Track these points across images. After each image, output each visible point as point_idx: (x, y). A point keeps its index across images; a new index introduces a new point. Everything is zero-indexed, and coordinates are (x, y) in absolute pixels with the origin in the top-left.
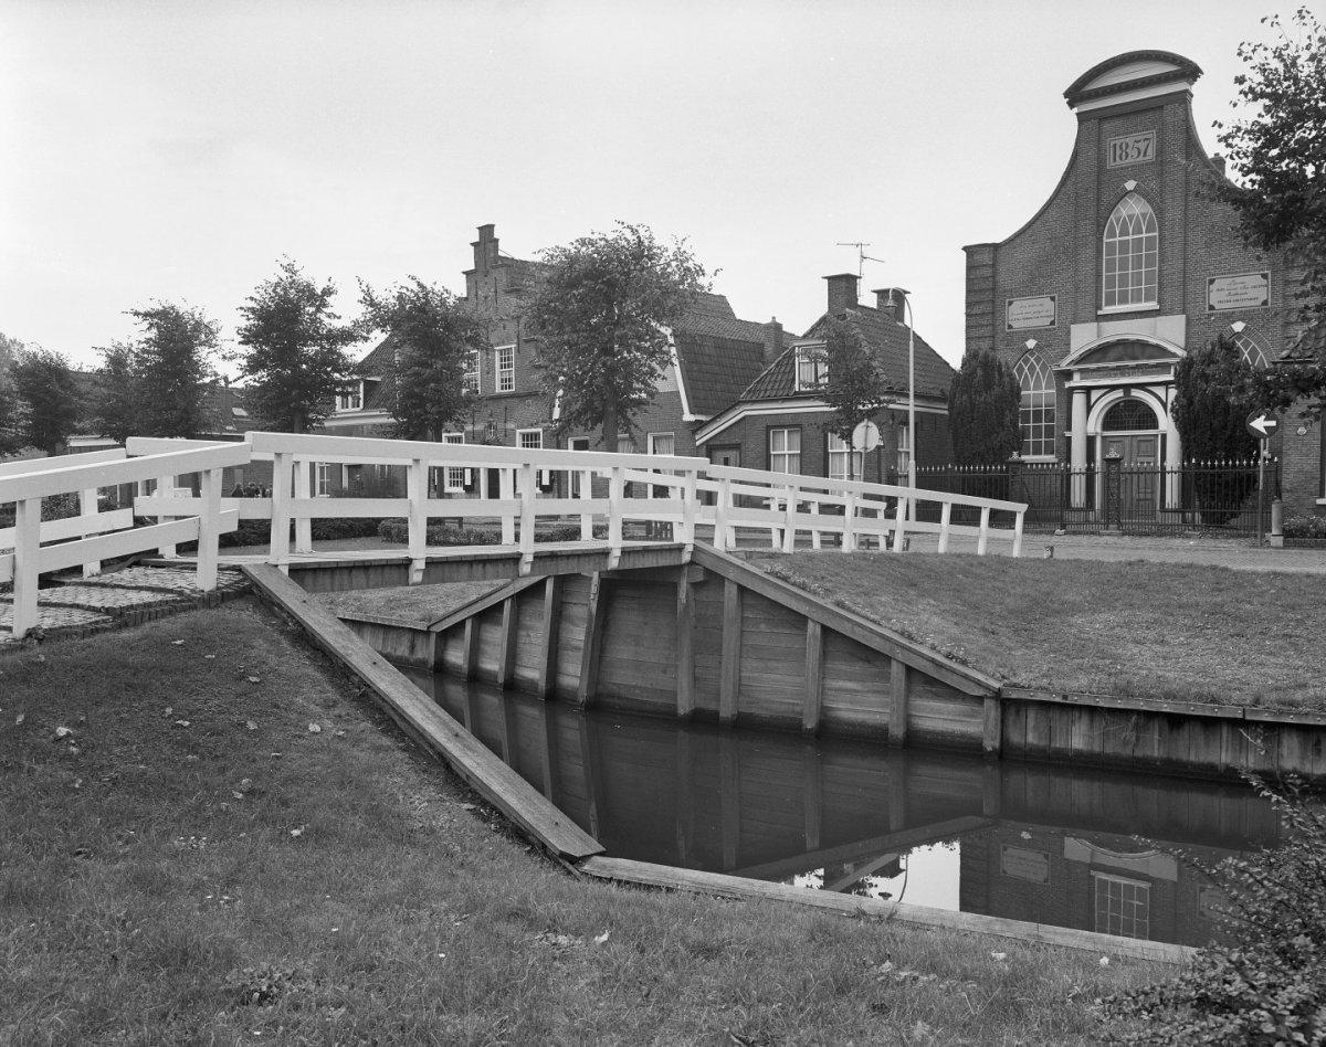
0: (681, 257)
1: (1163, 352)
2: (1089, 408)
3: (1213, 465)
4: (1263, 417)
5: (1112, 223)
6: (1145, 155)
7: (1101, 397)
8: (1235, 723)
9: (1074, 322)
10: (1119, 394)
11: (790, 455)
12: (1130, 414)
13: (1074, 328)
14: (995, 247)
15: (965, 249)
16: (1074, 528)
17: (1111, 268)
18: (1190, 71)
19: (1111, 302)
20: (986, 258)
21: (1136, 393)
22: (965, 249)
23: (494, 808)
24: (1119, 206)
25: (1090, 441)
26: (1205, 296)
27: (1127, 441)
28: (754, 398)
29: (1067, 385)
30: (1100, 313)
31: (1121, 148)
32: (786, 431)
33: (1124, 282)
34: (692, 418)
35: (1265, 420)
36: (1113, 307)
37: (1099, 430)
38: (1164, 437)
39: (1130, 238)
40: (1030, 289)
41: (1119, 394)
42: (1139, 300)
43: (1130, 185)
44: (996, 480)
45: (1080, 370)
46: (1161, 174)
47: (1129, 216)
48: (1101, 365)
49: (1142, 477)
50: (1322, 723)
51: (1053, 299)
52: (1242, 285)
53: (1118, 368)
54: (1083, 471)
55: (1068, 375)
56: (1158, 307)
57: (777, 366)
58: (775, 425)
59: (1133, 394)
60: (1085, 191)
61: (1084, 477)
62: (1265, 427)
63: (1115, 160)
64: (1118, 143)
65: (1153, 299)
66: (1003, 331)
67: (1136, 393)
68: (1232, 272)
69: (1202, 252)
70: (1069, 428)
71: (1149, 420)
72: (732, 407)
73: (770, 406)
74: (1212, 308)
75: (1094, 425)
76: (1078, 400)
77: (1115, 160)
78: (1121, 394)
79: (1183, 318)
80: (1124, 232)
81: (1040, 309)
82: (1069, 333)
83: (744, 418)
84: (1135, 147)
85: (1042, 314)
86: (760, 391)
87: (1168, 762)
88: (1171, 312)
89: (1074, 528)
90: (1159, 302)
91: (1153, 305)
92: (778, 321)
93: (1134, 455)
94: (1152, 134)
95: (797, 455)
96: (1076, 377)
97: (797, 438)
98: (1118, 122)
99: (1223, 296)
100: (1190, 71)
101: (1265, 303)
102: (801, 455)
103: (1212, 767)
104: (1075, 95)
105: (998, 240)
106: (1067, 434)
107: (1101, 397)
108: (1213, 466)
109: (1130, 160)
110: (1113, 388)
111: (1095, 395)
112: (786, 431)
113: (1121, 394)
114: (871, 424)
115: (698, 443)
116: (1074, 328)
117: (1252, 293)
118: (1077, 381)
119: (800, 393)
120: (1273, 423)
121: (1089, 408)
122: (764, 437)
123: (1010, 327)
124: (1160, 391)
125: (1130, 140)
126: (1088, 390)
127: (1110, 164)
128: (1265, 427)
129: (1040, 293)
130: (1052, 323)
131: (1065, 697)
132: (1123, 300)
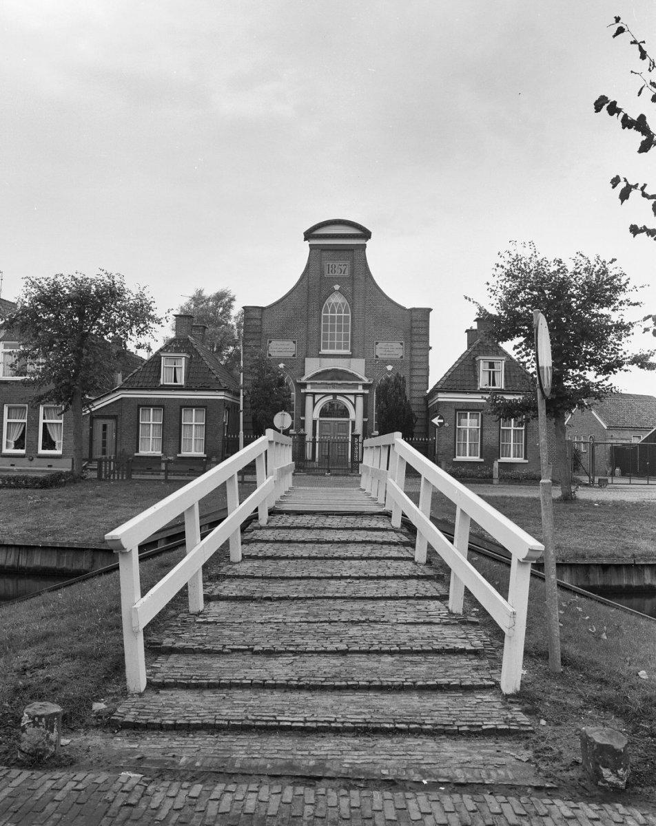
0: (141, 296)
2: (314, 405)
5: (326, 306)
7: (321, 398)
8: (628, 566)
9: (307, 357)
10: (330, 398)
11: (196, 425)
12: (334, 410)
13: (307, 360)
14: (263, 309)
16: (335, 472)
17: (326, 329)
18: (366, 235)
19: (325, 348)
20: (257, 314)
21: (339, 398)
23: (227, 653)
25: (314, 422)
27: (332, 424)
29: (303, 391)
30: (320, 353)
31: (332, 267)
32: (152, 409)
33: (332, 338)
37: (318, 417)
38: (354, 423)
39: (336, 315)
40: (282, 335)
41: (330, 398)
42: (334, 348)
45: (311, 383)
46: (353, 285)
48: (322, 381)
49: (340, 444)
50: (655, 563)
51: (294, 342)
53: (332, 384)
54: (311, 440)
55: (304, 385)
58: (147, 404)
60: (311, 288)
63: (329, 273)
64: (331, 264)
65: (348, 349)
69: (372, 327)
70: (303, 415)
71: (345, 413)
73: (129, 392)
74: (377, 357)
75: (316, 415)
76: (309, 400)
77: (329, 273)
78: (332, 398)
80: (333, 311)
81: (288, 347)
82: (304, 362)
83: (121, 398)
84: (340, 268)
87: (603, 586)
88: (358, 357)
89: (335, 472)
91: (347, 352)
94: (348, 263)
100: (366, 235)
101: (402, 357)
103: (620, 587)
104: (308, 235)
105: (264, 305)
107: (321, 398)
111: (317, 397)
112: (194, 410)
113: (332, 398)
114: (286, 413)
116: (307, 360)
118: (309, 389)
120: (442, 421)
121: (314, 405)
124: (352, 398)
125: (337, 264)
126: (314, 394)
127: (326, 275)
129: (287, 338)
130: (294, 356)
131: (563, 561)
132: (339, 348)
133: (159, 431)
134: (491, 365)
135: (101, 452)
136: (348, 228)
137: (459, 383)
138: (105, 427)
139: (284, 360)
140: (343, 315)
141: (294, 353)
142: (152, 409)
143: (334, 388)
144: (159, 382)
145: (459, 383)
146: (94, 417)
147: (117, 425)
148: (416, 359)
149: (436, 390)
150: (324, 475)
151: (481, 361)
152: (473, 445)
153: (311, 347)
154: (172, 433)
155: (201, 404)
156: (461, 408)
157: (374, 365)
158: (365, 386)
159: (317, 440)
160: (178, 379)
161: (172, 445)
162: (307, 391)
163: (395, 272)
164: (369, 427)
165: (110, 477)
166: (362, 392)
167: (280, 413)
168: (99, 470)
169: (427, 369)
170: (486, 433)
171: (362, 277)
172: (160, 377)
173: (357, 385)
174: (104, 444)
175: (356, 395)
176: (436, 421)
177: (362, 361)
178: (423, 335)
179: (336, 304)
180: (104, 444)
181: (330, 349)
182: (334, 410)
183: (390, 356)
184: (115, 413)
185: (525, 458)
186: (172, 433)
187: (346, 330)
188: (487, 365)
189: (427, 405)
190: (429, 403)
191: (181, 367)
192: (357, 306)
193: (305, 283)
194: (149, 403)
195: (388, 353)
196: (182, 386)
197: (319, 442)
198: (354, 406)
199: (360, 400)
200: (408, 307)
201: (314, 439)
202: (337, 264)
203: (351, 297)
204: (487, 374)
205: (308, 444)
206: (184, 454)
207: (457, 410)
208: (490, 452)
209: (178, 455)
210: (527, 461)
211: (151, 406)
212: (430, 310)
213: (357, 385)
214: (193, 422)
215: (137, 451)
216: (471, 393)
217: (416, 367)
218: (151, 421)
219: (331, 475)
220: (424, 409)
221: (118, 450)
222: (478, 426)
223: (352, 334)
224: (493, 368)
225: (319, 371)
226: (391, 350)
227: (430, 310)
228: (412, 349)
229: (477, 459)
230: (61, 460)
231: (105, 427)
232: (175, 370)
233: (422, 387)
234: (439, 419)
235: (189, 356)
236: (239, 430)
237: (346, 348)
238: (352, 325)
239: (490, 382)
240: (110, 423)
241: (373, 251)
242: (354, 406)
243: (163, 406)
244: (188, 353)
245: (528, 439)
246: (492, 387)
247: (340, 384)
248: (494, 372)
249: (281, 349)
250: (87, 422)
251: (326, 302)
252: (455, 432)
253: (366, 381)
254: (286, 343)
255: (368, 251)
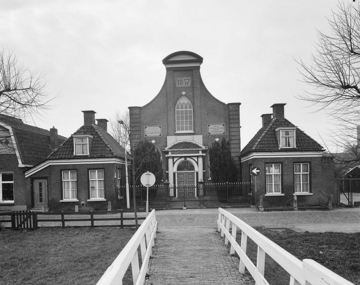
1: (196, 146)
2: (174, 164)
3: (235, 184)
4: (256, 169)
6: (188, 84)
9: (168, 135)
10: (183, 159)
11: (99, 180)
12: (185, 166)
13: (168, 137)
15: (129, 108)
19: (179, 130)
20: (137, 111)
21: (188, 159)
22: (129, 108)
24: (180, 99)
25: (174, 174)
26: (207, 130)
27: (185, 174)
28: (54, 158)
29: (166, 156)
30: (176, 133)
32: (69, 172)
34: (23, 166)
35: (257, 170)
36: (188, 131)
37: (176, 171)
38: (197, 173)
40: (152, 123)
41: (183, 159)
43: (184, 93)
44: (153, 190)
45: (171, 151)
46: (193, 91)
47: (183, 103)
51: (160, 127)
52: (218, 127)
54: (173, 187)
55: (167, 153)
56: (194, 132)
57: (64, 144)
58: (66, 168)
59: (187, 159)
60: (169, 93)
61: (173, 189)
62: (257, 172)
63: (178, 85)
66: (144, 137)
67: (188, 159)
68: (214, 123)
70: (168, 170)
72: (44, 161)
74: (209, 133)
75: (175, 169)
76: (170, 161)
78: (184, 159)
79: (202, 136)
80: (182, 108)
82: (166, 138)
84: (185, 81)
85: (157, 132)
86: (57, 155)
90: (194, 131)
91: (192, 131)
92: (56, 128)
93: (187, 179)
94: (190, 78)
95: (103, 180)
96: (170, 153)
97: (75, 175)
98: (179, 73)
99: (212, 130)
100: (199, 60)
101: (224, 133)
102: (77, 181)
104: (166, 61)
105: (141, 106)
106: (167, 172)
108: (222, 185)
109: (183, 85)
110: (181, 157)
112: (97, 171)
114: (150, 173)
115: (26, 177)
116: (168, 137)
117: (221, 130)
118: (170, 155)
119: (76, 156)
120: (259, 171)
121: (174, 164)
122: (59, 174)
123: (146, 136)
124: (196, 159)
125: (183, 79)
126: (173, 158)
127: (177, 86)
128: (257, 172)
129: (155, 125)
130: (160, 135)
132: (183, 130)
133: (75, 184)
134: (287, 133)
135: (39, 200)
136: (189, 57)
137: (266, 146)
138: (40, 184)
139: (155, 138)
140: (188, 109)
141: (160, 134)
142: (69, 172)
143: (185, 153)
144: (73, 154)
145: (266, 146)
146: (33, 178)
147: (48, 182)
148: (233, 134)
149: (249, 150)
150: (182, 209)
151: (281, 130)
152: (276, 186)
153: (169, 131)
154: (83, 186)
155: (101, 167)
156: (268, 161)
157: (207, 138)
158: (203, 151)
159: (177, 187)
160: (85, 151)
161: (83, 194)
162: (169, 156)
163: (219, 83)
164: (207, 175)
165: (21, 226)
166: (202, 155)
167: (146, 173)
168: (13, 221)
169: (239, 139)
170: (285, 177)
171: (198, 86)
172: (73, 151)
173: (199, 150)
174: (41, 195)
175: (198, 157)
176: (255, 171)
177: (201, 136)
178: (237, 119)
179: (184, 103)
180: (41, 195)
181: (181, 130)
182: (185, 166)
183: (217, 133)
184: (47, 176)
185: (311, 192)
186: (83, 186)
187: (190, 118)
188: (284, 133)
189: (240, 161)
190: (242, 160)
191: (87, 144)
192: (196, 104)
193: (245, 219)
194: (68, 168)
195: (216, 131)
196: (88, 156)
197: (178, 188)
198: (197, 163)
199: (200, 160)
200: (226, 103)
201: (175, 186)
202: (183, 79)
203: (192, 99)
204: (284, 139)
205: (171, 189)
206: (92, 199)
207: (266, 163)
208: (288, 188)
209: (88, 200)
210: (312, 194)
211: (69, 170)
212: (240, 104)
213: (199, 150)
214: (96, 179)
215: (62, 199)
216: (275, 151)
217: (233, 138)
218: (69, 179)
219: (187, 209)
220: (239, 163)
221: (50, 199)
222: (279, 172)
223: (194, 120)
224: (288, 135)
225: (176, 143)
226: (217, 129)
227: (240, 104)
228: (230, 128)
229: (279, 194)
230: (14, 206)
231: (40, 184)
232: (82, 148)
233: (236, 150)
234: (257, 170)
235: (92, 137)
236: (126, 183)
237: (191, 129)
238: (194, 115)
239: (286, 144)
240: (44, 182)
241: (205, 71)
242: (197, 163)
243: (76, 170)
244: (92, 135)
245: (312, 180)
246: (288, 147)
247: (188, 151)
248: (288, 137)
249: (152, 132)
250: (29, 181)
251: (178, 102)
252: (264, 176)
253: (204, 148)
254: (156, 128)
255: (201, 70)
